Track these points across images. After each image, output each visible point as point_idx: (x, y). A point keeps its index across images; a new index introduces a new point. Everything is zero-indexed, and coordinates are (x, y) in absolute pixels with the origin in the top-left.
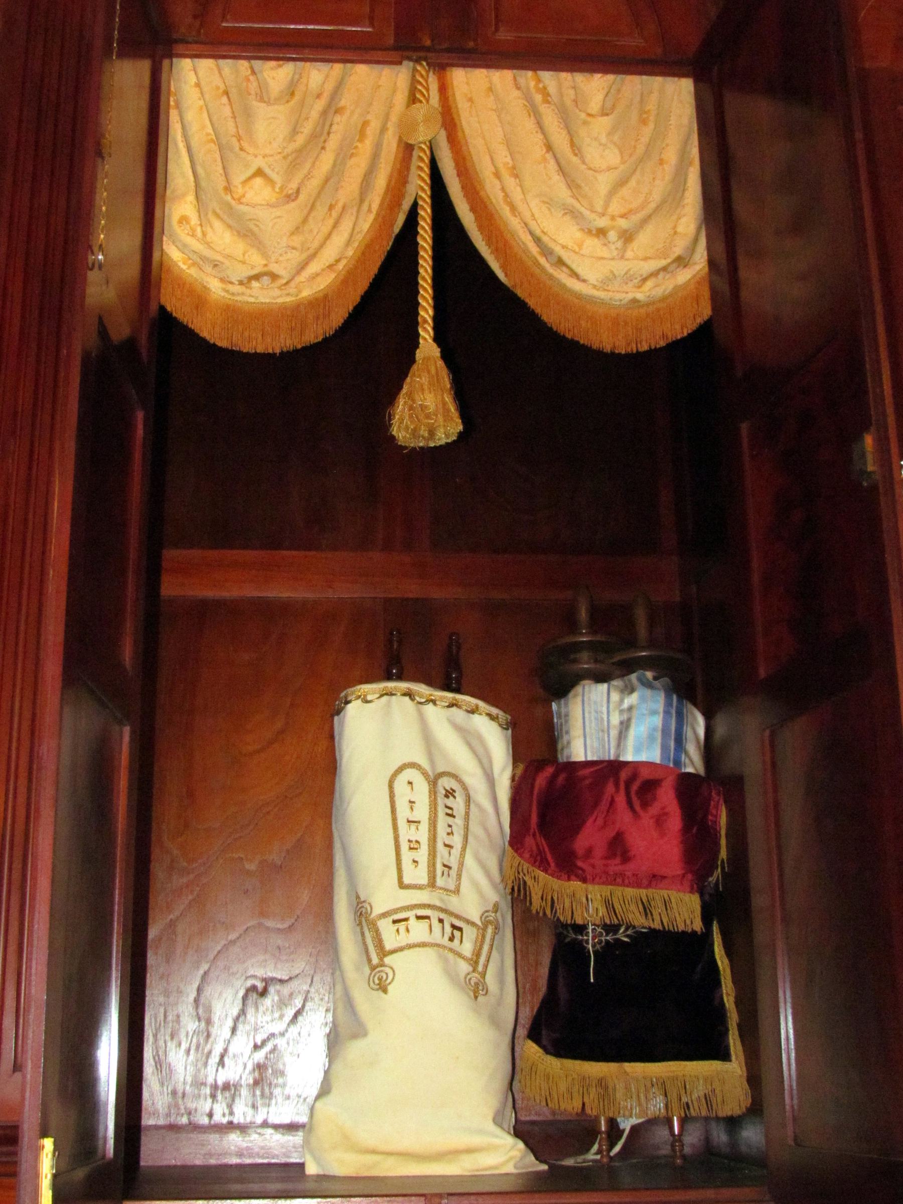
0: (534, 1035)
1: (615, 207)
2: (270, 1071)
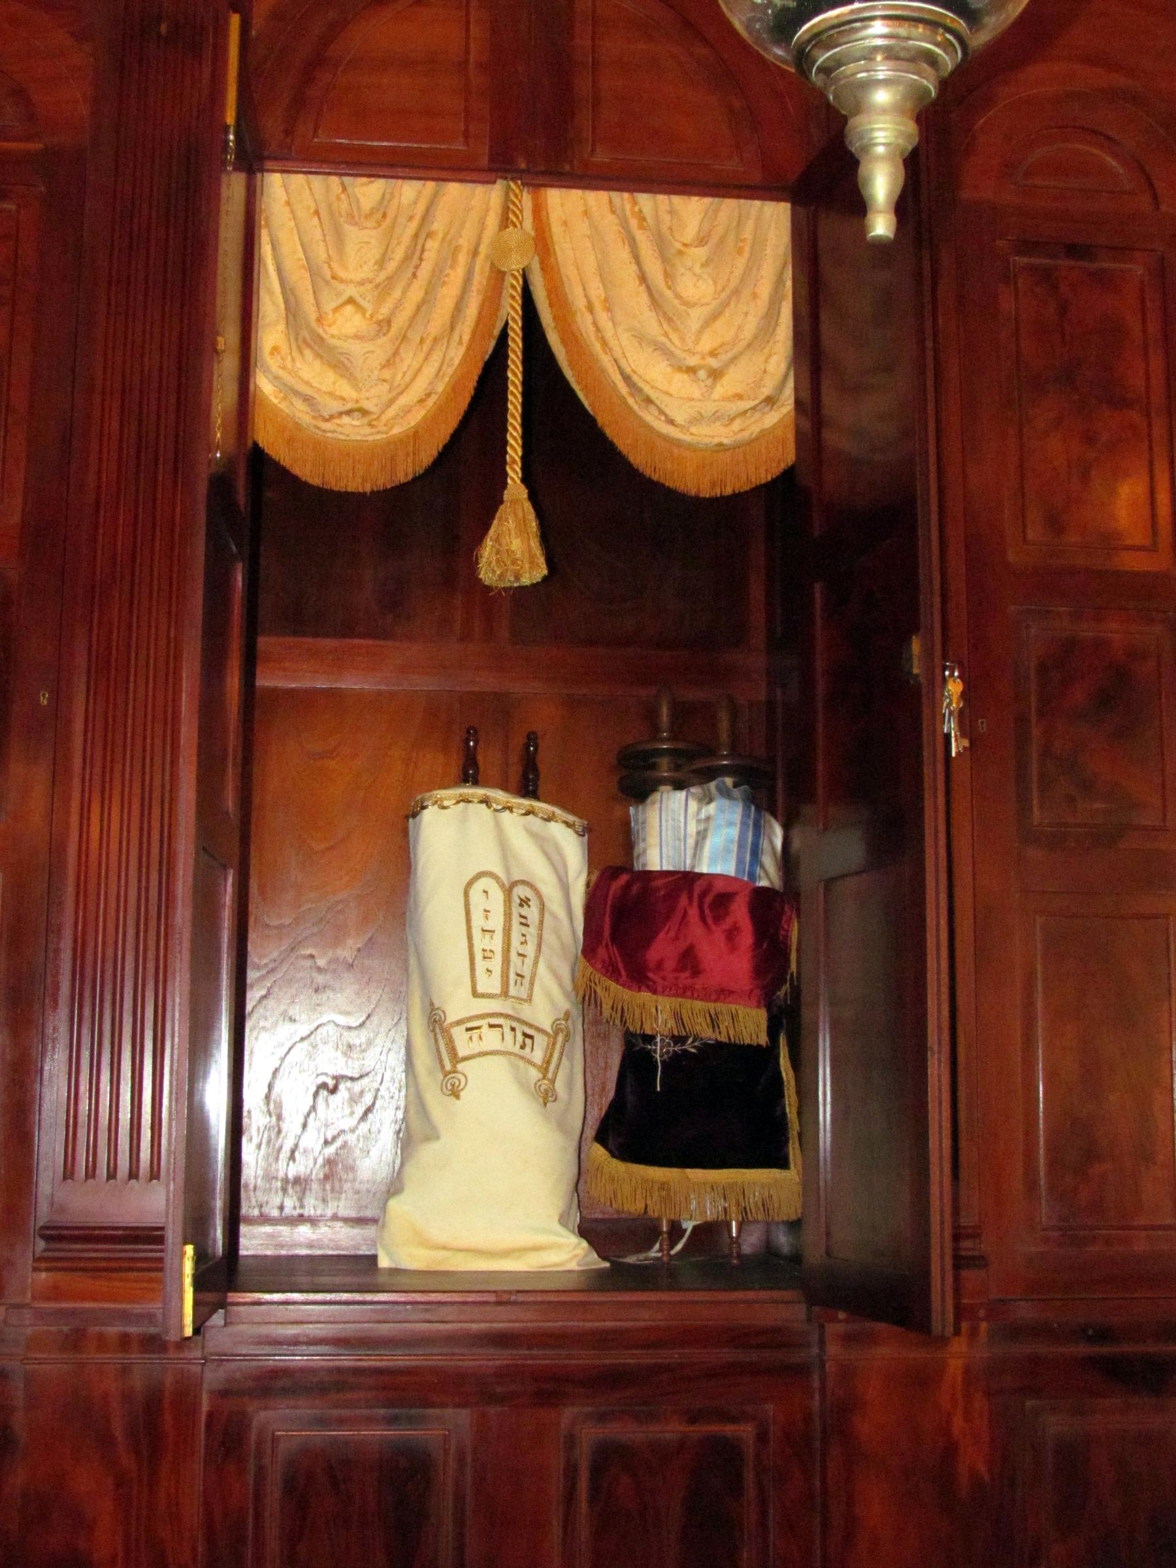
0: (601, 1137)
1: (706, 344)
2: (340, 1166)
